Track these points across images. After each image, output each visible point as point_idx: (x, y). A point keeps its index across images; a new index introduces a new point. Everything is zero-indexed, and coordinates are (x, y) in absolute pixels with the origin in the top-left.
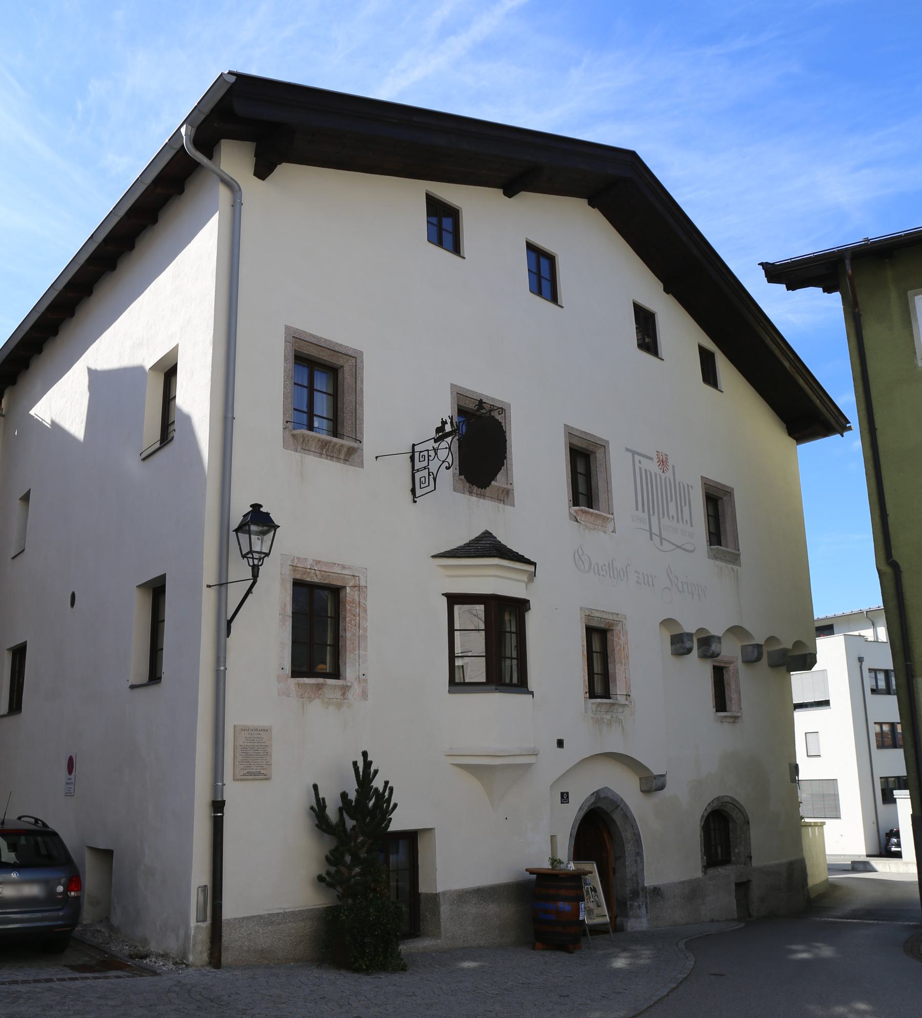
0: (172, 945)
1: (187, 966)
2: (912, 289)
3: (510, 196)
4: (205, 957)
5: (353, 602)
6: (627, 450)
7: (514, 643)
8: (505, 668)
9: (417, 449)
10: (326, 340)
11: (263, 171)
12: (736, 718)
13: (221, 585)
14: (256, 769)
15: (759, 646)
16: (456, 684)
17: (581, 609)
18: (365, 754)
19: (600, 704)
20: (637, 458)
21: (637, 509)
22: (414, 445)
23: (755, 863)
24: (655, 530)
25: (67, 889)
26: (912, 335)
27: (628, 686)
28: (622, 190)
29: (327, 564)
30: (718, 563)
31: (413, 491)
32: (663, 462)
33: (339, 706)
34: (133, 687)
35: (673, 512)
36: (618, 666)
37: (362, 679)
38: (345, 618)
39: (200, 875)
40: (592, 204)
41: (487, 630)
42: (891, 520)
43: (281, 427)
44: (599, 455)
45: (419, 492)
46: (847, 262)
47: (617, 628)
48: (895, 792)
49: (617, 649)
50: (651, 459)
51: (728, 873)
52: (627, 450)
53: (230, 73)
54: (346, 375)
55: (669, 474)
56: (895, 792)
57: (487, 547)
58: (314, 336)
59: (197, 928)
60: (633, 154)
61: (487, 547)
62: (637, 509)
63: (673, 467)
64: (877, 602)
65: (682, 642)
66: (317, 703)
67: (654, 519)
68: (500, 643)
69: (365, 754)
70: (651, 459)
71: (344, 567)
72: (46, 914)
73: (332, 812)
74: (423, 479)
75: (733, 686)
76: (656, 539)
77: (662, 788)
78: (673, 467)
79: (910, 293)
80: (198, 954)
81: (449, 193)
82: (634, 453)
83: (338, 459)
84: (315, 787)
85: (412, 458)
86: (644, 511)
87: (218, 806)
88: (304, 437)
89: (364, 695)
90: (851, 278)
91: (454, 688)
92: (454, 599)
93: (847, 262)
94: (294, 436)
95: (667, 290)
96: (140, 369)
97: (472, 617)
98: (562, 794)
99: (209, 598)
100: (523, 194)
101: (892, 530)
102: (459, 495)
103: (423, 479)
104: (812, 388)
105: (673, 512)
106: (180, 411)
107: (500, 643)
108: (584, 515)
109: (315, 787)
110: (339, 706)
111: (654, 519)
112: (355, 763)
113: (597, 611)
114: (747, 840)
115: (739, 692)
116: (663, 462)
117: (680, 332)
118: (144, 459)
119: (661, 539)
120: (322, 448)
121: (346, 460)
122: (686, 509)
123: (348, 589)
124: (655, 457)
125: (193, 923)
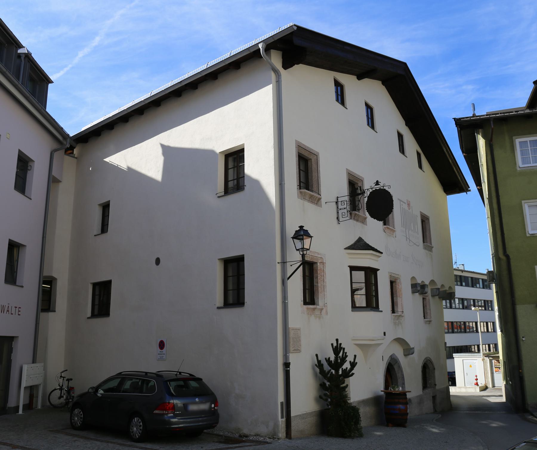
0: (263, 430)
1: (278, 439)
2: (515, 135)
4: (285, 434)
5: (321, 270)
7: (374, 289)
9: (340, 200)
10: (308, 147)
11: (287, 65)
12: (430, 321)
13: (284, 263)
15: (439, 289)
16: (354, 307)
18: (337, 340)
20: (401, 203)
22: (338, 197)
23: (437, 387)
24: (408, 237)
25: (215, 406)
26: (515, 156)
28: (397, 80)
31: (338, 218)
32: (409, 205)
33: (320, 318)
34: (218, 308)
35: (412, 228)
36: (398, 298)
37: (325, 305)
38: (317, 277)
39: (281, 398)
40: (383, 84)
42: (506, 236)
45: (341, 219)
46: (492, 122)
47: (398, 281)
48: (454, 354)
49: (398, 290)
50: (405, 203)
51: (429, 391)
53: (295, 25)
54: (313, 163)
56: (454, 354)
57: (360, 245)
58: (304, 145)
59: (282, 421)
60: (405, 64)
61: (360, 245)
65: (417, 287)
67: (407, 230)
68: (368, 290)
69: (337, 340)
70: (405, 203)
72: (192, 420)
73: (326, 367)
74: (344, 214)
75: (428, 307)
76: (408, 240)
77: (412, 354)
79: (514, 137)
80: (282, 434)
81: (343, 78)
82: (400, 201)
84: (317, 355)
85: (337, 203)
87: (287, 365)
88: (305, 193)
90: (492, 129)
91: (354, 309)
92: (353, 268)
93: (492, 122)
94: (301, 192)
95: (406, 125)
96: (212, 152)
97: (360, 276)
99: (279, 267)
100: (300, 65)
101: (506, 241)
103: (344, 214)
104: (458, 172)
105: (412, 228)
106: (250, 177)
109: (317, 355)
111: (407, 230)
112: (332, 344)
114: (434, 377)
115: (430, 310)
116: (409, 205)
117: (411, 144)
118: (219, 197)
119: (410, 240)
120: (310, 198)
122: (416, 226)
123: (318, 264)
124: (406, 202)
125: (280, 419)
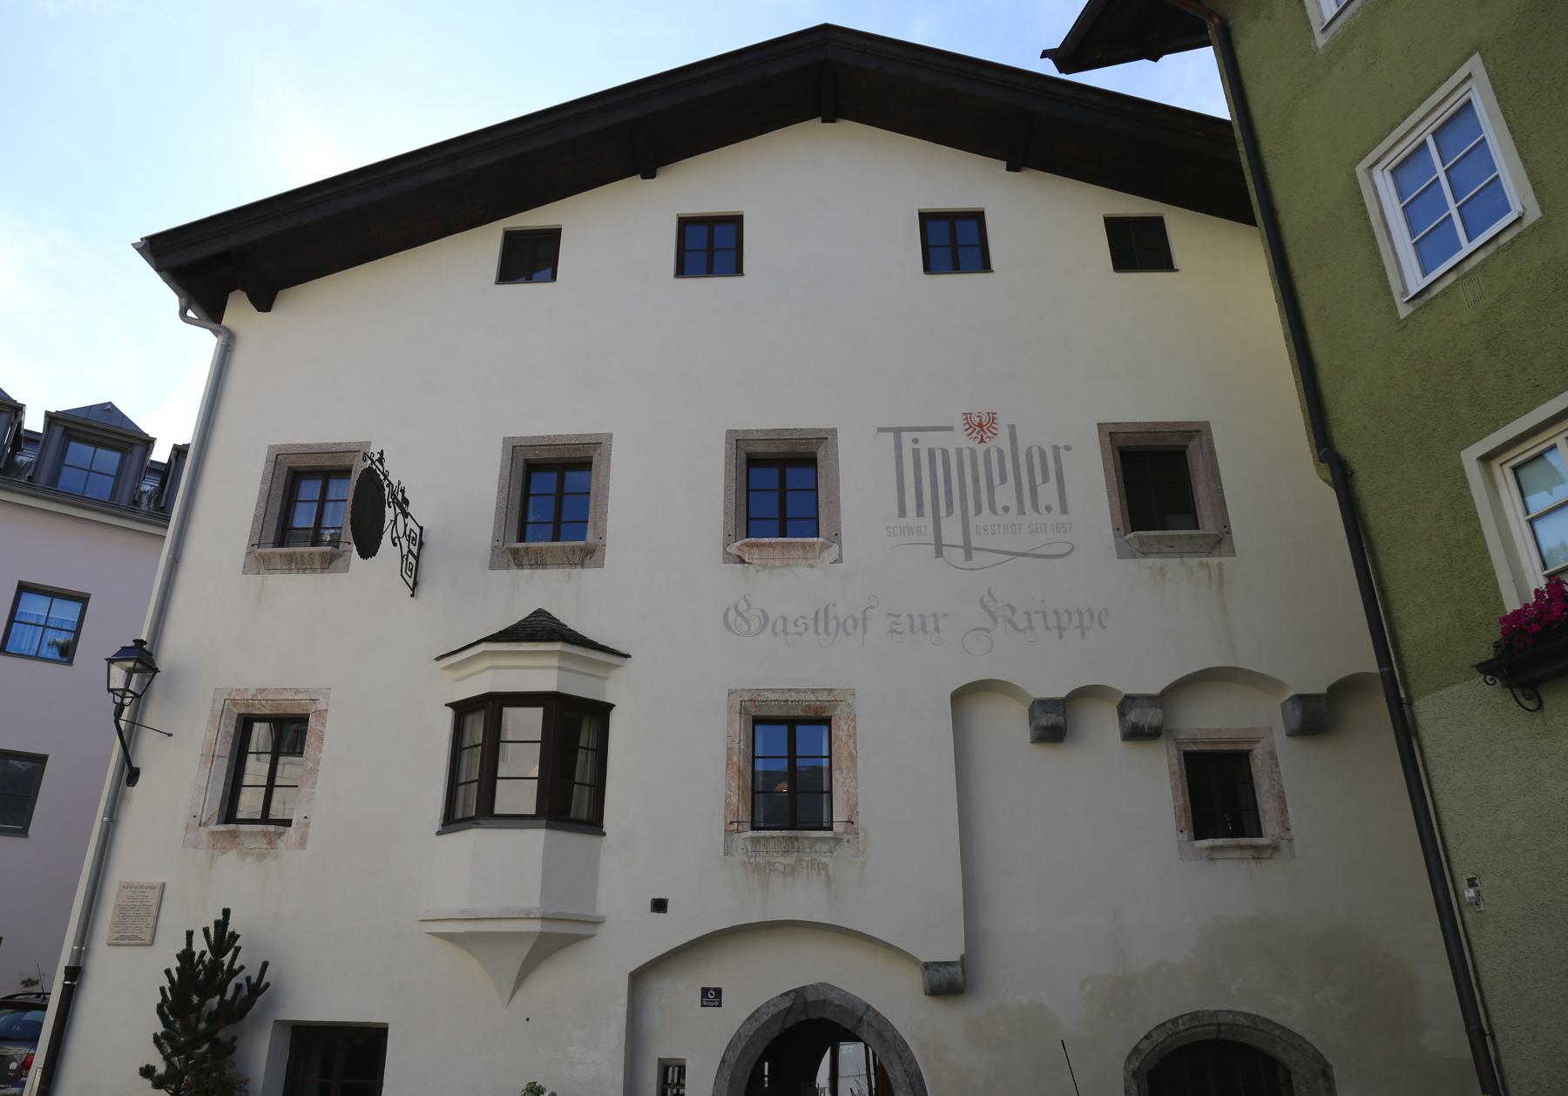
3: (653, 176)
6: (880, 430)
8: (572, 792)
14: (138, 931)
17: (731, 693)
19: (1213, 848)
21: (902, 512)
27: (853, 809)
29: (276, 690)
30: (1148, 562)
40: (830, 118)
41: (544, 742)
43: (244, 552)
44: (1196, 463)
52: (880, 430)
55: (1002, 441)
57: (539, 629)
62: (902, 512)
63: (1012, 428)
64: (777, 515)
66: (232, 855)
71: (298, 691)
78: (1012, 428)
83: (313, 570)
86: (920, 513)
89: (302, 843)
98: (705, 991)
102: (500, 574)
107: (543, 755)
108: (755, 550)
110: (261, 857)
113: (773, 691)
119: (968, 551)
120: (290, 562)
121: (323, 569)
